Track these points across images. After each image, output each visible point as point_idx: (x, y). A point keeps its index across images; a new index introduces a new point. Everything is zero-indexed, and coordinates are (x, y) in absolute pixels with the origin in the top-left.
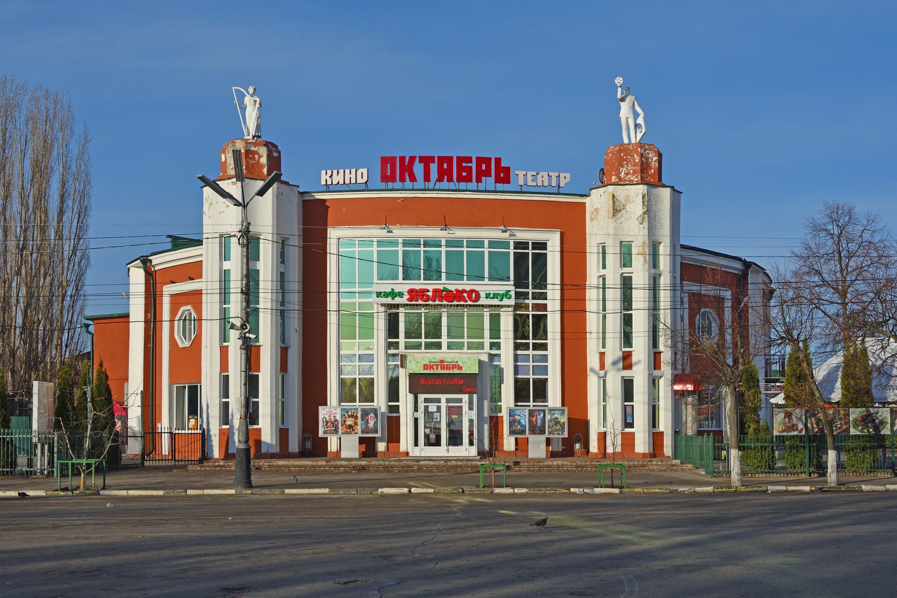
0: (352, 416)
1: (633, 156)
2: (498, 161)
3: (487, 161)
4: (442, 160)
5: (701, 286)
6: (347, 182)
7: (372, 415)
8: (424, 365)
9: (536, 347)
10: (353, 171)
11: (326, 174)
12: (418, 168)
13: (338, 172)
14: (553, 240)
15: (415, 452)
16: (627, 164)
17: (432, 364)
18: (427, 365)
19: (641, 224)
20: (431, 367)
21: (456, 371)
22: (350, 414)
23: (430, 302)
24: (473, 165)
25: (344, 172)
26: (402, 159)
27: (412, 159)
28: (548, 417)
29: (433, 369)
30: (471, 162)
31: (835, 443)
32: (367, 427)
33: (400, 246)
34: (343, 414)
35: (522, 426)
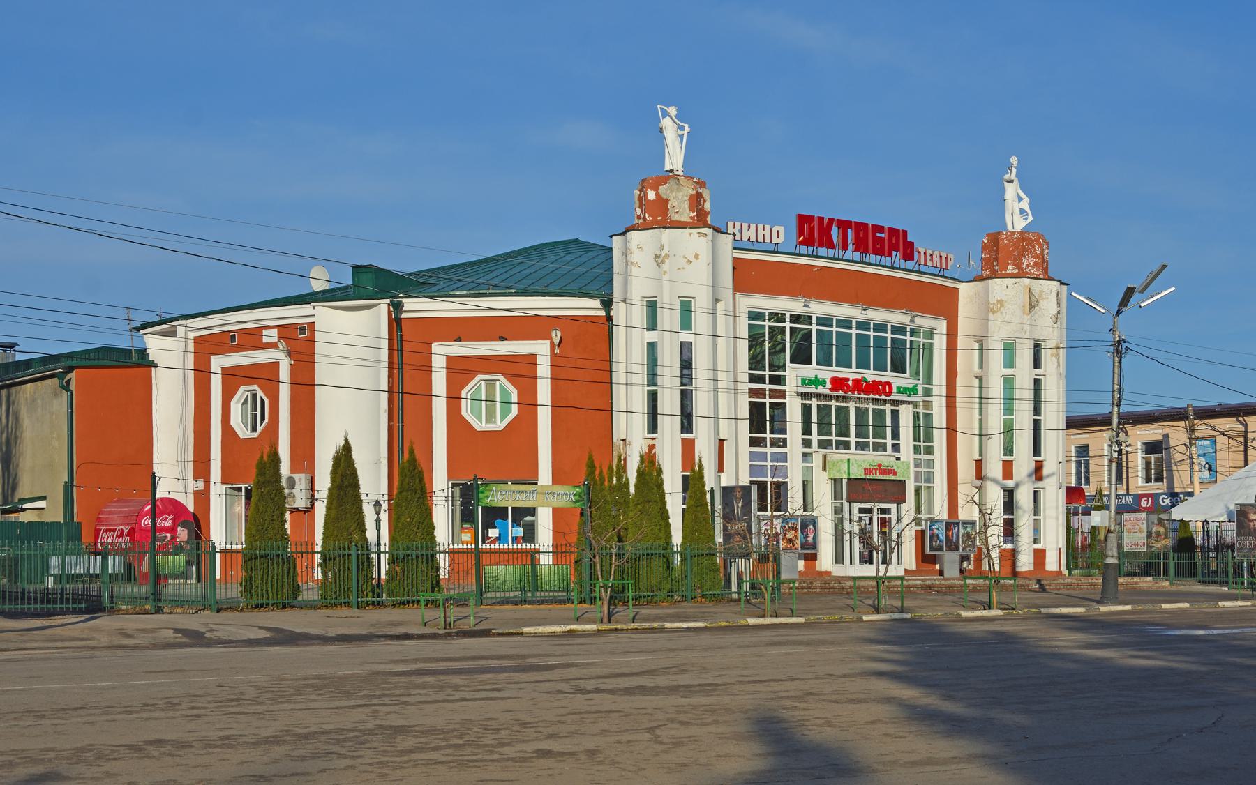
0: (792, 528)
1: (1034, 247)
2: (905, 232)
5: (1045, 390)
6: (760, 239)
7: (811, 527)
9: (774, 443)
10: (767, 227)
11: (734, 227)
12: (835, 233)
13: (749, 227)
15: (838, 571)
16: (1028, 255)
17: (872, 467)
18: (867, 469)
19: (1056, 323)
20: (871, 472)
21: (892, 477)
22: (790, 525)
23: (850, 394)
25: (757, 227)
26: (821, 219)
27: (831, 220)
28: (962, 531)
31: (358, 597)
32: (807, 541)
33: (854, 329)
34: (783, 525)
35: (940, 541)
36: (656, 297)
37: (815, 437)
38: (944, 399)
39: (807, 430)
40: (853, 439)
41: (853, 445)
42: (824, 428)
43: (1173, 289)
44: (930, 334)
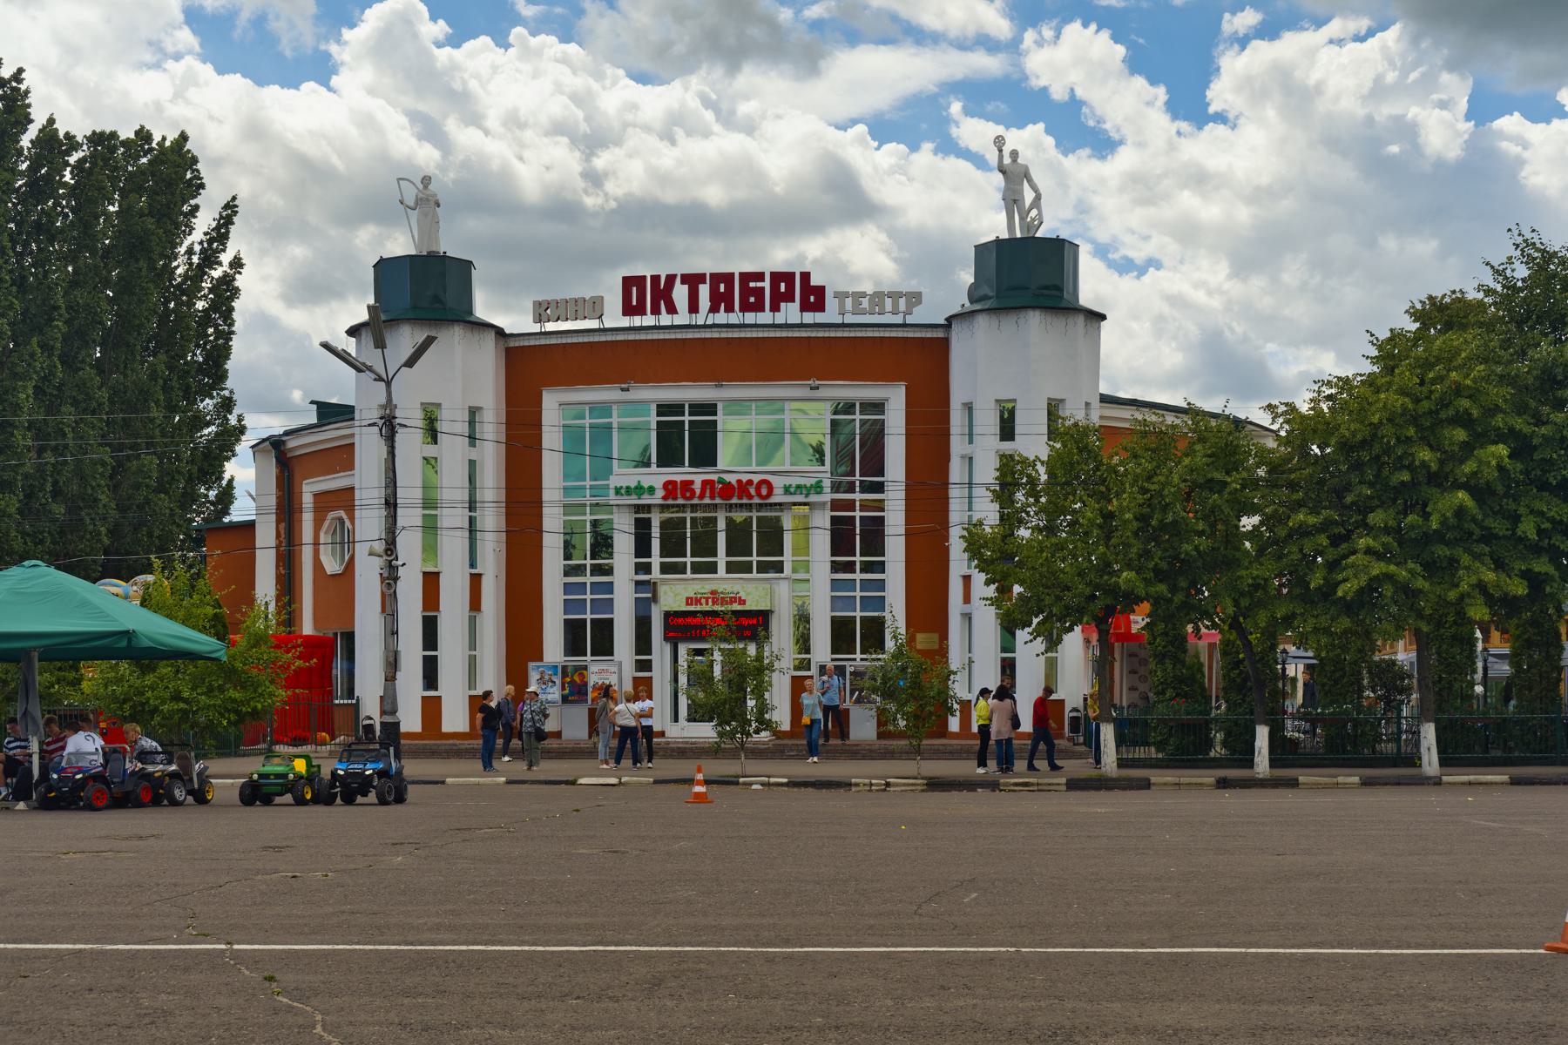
2: (806, 276)
3: (788, 277)
4: (717, 278)
8: (687, 599)
14: (895, 399)
17: (699, 596)
20: (698, 601)
21: (736, 607)
24: (766, 284)
27: (671, 279)
29: (701, 604)
30: (763, 280)
36: (1015, 401)
37: (656, 560)
38: (357, 503)
39: (642, 548)
40: (722, 559)
41: (722, 567)
42: (672, 546)
43: (634, 303)
44: (878, 407)
